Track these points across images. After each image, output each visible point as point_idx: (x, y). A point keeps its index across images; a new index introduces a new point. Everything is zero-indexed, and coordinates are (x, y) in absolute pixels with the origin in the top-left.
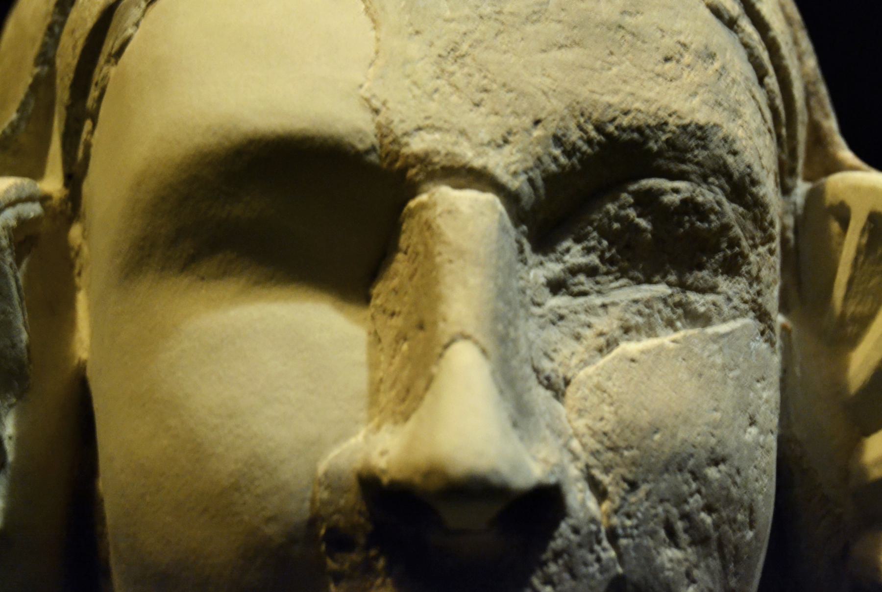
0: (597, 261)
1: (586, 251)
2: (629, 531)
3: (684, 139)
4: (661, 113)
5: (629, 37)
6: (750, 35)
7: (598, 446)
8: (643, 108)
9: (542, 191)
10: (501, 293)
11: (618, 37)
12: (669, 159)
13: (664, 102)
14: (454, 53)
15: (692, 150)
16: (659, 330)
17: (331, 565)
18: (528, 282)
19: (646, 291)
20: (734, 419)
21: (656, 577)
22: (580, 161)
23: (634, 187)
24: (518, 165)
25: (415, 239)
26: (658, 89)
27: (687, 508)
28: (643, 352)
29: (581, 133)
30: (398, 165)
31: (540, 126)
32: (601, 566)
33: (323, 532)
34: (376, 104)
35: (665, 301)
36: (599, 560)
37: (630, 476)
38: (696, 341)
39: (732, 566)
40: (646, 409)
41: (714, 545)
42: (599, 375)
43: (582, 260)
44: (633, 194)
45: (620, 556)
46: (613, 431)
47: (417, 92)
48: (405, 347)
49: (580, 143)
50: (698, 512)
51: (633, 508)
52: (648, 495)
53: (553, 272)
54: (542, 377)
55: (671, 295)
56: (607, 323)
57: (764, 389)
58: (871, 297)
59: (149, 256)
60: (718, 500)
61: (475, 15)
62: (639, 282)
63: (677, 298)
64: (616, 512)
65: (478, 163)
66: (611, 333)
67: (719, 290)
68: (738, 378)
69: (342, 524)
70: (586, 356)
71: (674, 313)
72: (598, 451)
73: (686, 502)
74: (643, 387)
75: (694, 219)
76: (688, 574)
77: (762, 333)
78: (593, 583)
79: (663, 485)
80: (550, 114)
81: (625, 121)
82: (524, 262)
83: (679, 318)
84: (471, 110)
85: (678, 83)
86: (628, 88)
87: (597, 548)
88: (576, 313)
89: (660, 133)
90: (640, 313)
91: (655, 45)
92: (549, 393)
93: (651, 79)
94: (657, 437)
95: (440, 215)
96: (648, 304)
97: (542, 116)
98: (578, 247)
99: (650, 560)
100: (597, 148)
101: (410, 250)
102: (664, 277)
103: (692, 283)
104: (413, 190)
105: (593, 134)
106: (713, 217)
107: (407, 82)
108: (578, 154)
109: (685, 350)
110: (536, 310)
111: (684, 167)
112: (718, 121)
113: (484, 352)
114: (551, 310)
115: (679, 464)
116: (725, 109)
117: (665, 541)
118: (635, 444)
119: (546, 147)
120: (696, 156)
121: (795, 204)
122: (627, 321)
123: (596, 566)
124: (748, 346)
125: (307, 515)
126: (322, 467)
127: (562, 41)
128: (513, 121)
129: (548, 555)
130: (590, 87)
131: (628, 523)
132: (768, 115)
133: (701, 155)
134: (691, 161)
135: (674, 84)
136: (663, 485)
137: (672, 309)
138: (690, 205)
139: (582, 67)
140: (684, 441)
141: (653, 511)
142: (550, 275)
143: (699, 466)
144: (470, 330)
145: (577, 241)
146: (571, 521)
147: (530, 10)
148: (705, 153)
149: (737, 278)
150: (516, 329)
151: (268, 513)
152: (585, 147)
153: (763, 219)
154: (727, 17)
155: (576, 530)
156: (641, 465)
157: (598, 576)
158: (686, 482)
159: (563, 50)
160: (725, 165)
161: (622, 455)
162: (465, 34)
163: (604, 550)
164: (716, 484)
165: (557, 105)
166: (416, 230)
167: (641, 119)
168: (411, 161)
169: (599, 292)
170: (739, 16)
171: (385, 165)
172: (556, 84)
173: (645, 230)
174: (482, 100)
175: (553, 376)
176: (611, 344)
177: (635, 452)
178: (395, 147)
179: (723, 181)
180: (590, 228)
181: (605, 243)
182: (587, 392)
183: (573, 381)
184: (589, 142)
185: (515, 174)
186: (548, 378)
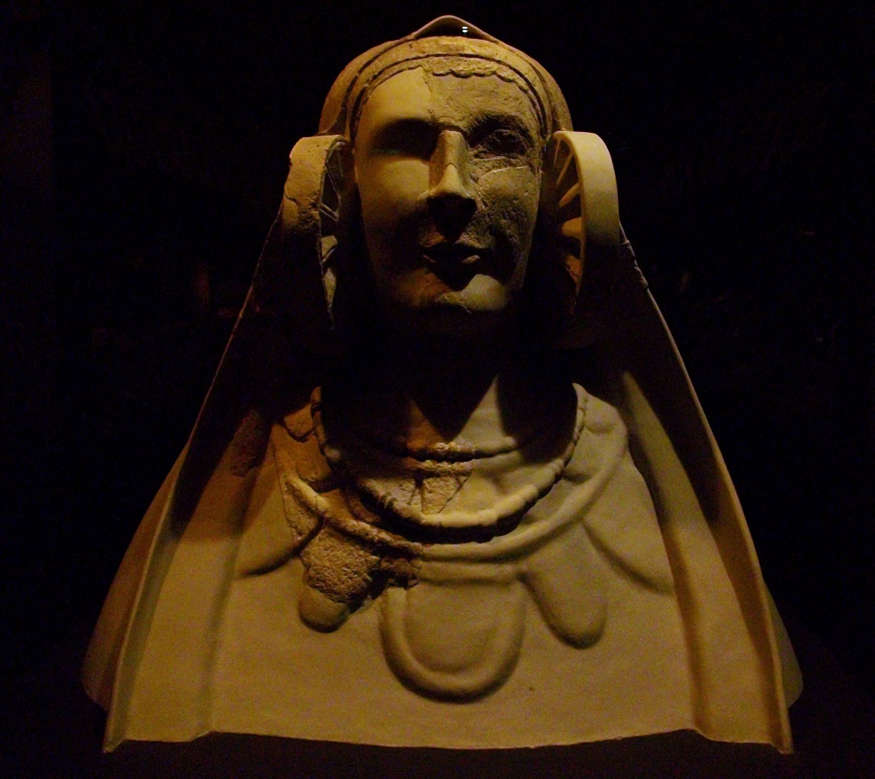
6: (531, 95)
9: (472, 132)
23: (496, 131)
34: (431, 111)
36: (485, 221)
43: (483, 150)
44: (496, 133)
52: (498, 206)
81: (493, 114)
82: (468, 149)
90: (497, 163)
96: (500, 160)
105: (485, 117)
109: (509, 172)
110: (471, 162)
126: (418, 199)
128: (465, 115)
131: (493, 212)
132: (536, 116)
133: (512, 123)
144: (452, 162)
152: (482, 121)
160: (520, 126)
176: (489, 170)
184: (484, 120)
186: (473, 178)
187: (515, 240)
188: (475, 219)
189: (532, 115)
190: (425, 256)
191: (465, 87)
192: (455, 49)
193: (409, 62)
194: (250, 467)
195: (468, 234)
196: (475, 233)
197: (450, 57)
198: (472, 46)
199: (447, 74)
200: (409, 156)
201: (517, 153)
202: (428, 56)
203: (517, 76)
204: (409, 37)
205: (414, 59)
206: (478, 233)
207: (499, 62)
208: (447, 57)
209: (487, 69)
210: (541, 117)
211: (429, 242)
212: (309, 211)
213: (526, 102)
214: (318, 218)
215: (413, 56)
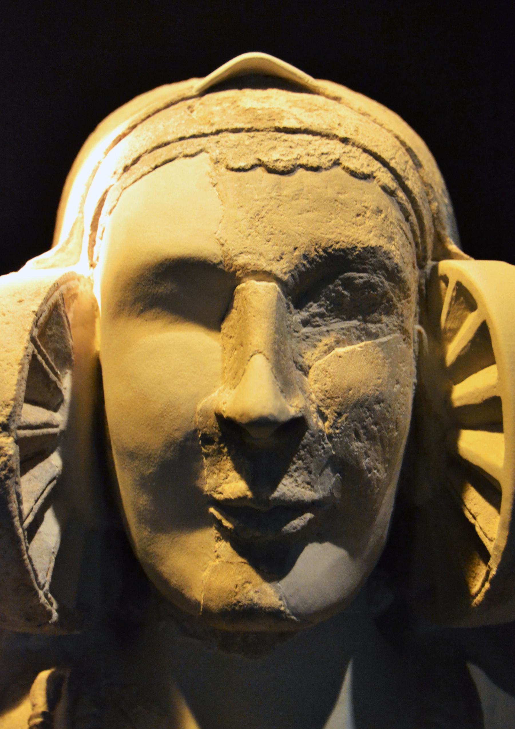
0: (324, 311)
1: (319, 306)
2: (337, 435)
3: (365, 253)
4: (354, 242)
5: (340, 205)
6: (401, 198)
7: (323, 397)
8: (345, 240)
9: (298, 280)
10: (277, 331)
11: (335, 205)
12: (358, 263)
13: (355, 237)
14: (258, 216)
15: (369, 259)
16: (354, 341)
17: (204, 450)
18: (292, 321)
19: (347, 324)
20: (388, 382)
21: (350, 455)
22: (316, 266)
23: (342, 276)
25: (240, 304)
26: (353, 230)
28: (345, 353)
29: (316, 253)
30: (232, 270)
31: (297, 250)
32: (325, 451)
33: (200, 436)
34: (222, 241)
35: (356, 328)
36: (323, 448)
37: (338, 410)
39: (387, 449)
43: (318, 310)
44: (341, 280)
47: (241, 236)
48: (236, 353)
49: (316, 257)
50: (370, 425)
52: (346, 418)
53: (304, 316)
54: (298, 365)
57: (404, 366)
58: (458, 320)
59: (123, 310)
61: (268, 197)
62: (344, 320)
63: (362, 327)
64: (331, 427)
65: (268, 269)
66: (330, 344)
67: (382, 322)
68: (390, 363)
69: (208, 433)
71: (361, 333)
72: (323, 399)
73: (364, 421)
74: (345, 369)
75: (370, 290)
76: (366, 453)
77: (404, 340)
78: (321, 458)
79: (354, 414)
80: (302, 245)
81: (337, 247)
82: (290, 313)
83: (363, 335)
84: (265, 244)
85: (363, 226)
86: (339, 231)
87: (322, 443)
88: (315, 335)
89: (353, 251)
90: (344, 334)
91: (352, 209)
92: (301, 373)
93: (349, 225)
94: (351, 392)
95: (250, 294)
96: (348, 329)
97: (298, 245)
98: (316, 305)
99: (347, 447)
100: (324, 260)
101: (238, 308)
104: (239, 281)
105: (322, 253)
106: (379, 289)
107: (237, 231)
108: (315, 263)
110: (296, 334)
111: (365, 267)
112: (381, 245)
113: (268, 359)
114: (303, 334)
116: (385, 238)
117: (354, 439)
118: (340, 396)
120: (370, 261)
121: (426, 273)
123: (322, 451)
124: (396, 347)
125: (193, 428)
126: (199, 407)
127: (309, 209)
128: (285, 249)
129: (300, 446)
130: (320, 231)
131: (337, 431)
132: (410, 235)
133: (373, 260)
135: (360, 227)
137: (360, 332)
139: (317, 221)
141: (349, 426)
142: (303, 318)
143: (371, 405)
144: (261, 349)
145: (315, 302)
146: (310, 432)
147: (294, 194)
148: (375, 260)
149: (391, 316)
150: (285, 345)
151: (176, 428)
152: (318, 259)
153: (404, 288)
154: (389, 190)
155: (313, 436)
157: (323, 455)
158: (365, 412)
159: (309, 213)
160: (385, 264)
161: (334, 401)
162: (263, 207)
163: (326, 444)
164: (378, 413)
166: (240, 300)
167: (344, 246)
168: (238, 268)
169: (326, 325)
170: (396, 189)
171: (226, 270)
172: (305, 230)
173: (347, 296)
174: (271, 239)
175: (303, 365)
176: (331, 349)
177: (340, 399)
178: (231, 262)
180: (321, 296)
181: (328, 302)
182: (319, 372)
186: (301, 366)
187: (378, 474)
188: (304, 447)
189: (404, 237)
190: (212, 510)
191: (284, 193)
192: (267, 117)
193: (185, 142)
195: (291, 476)
196: (305, 473)
197: (257, 133)
198: (295, 111)
199: (253, 167)
202: (218, 132)
203: (377, 165)
205: (194, 136)
206: (310, 472)
207: (345, 141)
208: (252, 134)
210: (418, 233)
211: (220, 489)
213: (395, 214)
214: (11, 452)
215: (193, 131)
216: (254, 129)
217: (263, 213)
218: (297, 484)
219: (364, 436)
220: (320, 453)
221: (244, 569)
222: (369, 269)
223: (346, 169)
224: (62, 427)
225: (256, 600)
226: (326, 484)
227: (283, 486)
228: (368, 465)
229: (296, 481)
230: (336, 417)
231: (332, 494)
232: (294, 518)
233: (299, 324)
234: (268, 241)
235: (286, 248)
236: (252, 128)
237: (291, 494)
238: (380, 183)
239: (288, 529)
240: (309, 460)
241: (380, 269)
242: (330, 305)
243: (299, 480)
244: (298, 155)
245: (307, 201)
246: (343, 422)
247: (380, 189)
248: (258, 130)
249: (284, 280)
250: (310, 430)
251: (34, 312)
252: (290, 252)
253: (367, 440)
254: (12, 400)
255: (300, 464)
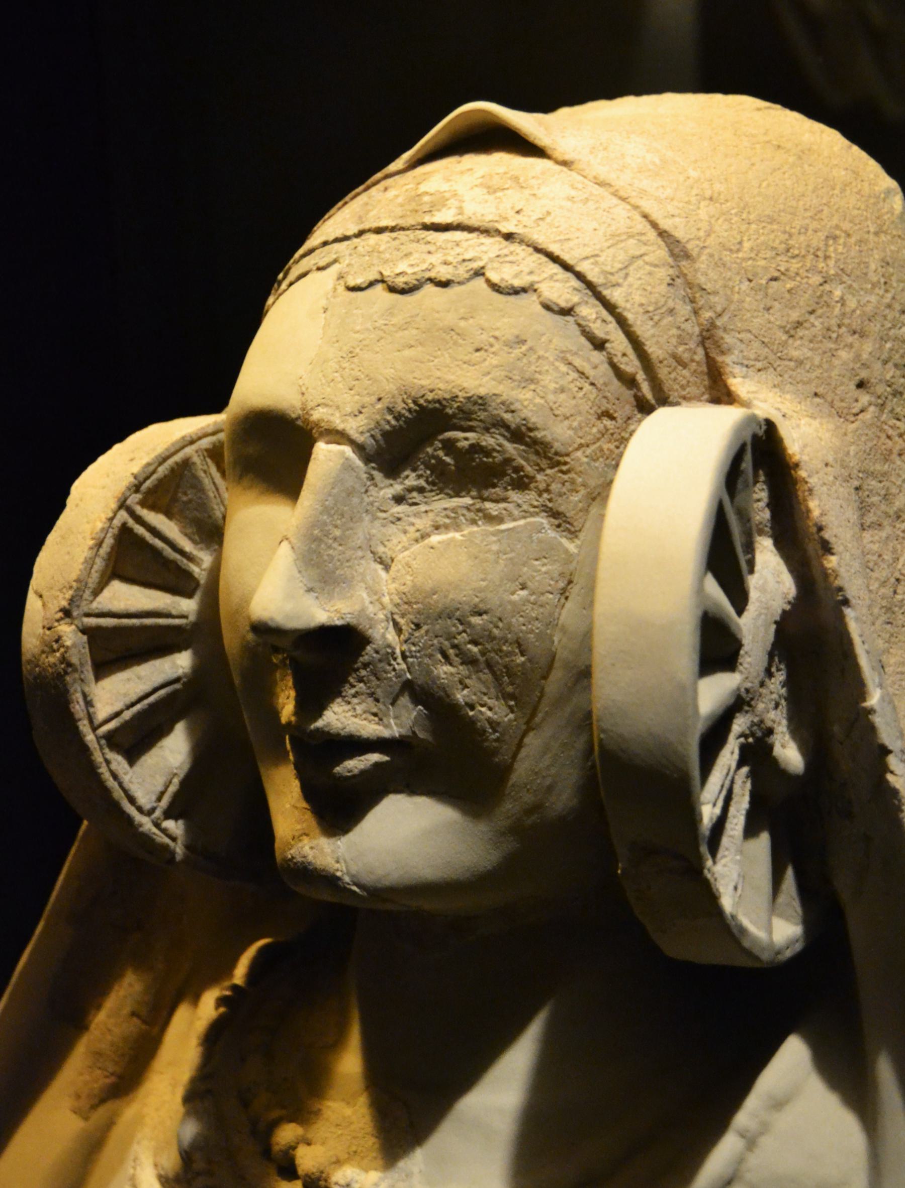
2: (414, 654)
3: (469, 406)
7: (399, 601)
9: (382, 442)
12: (460, 419)
13: (459, 382)
15: (476, 413)
18: (378, 497)
19: (454, 502)
22: (405, 422)
23: (441, 437)
24: (364, 427)
27: (456, 641)
28: (439, 543)
29: (404, 405)
30: (309, 427)
32: (396, 674)
36: (394, 670)
37: (415, 621)
38: (477, 535)
40: (431, 579)
41: (483, 666)
42: (409, 557)
43: (415, 483)
45: (409, 668)
46: (409, 592)
49: (404, 412)
50: (466, 645)
51: (417, 640)
52: (427, 632)
54: (376, 557)
55: (473, 504)
56: (423, 523)
60: (481, 638)
62: (451, 497)
63: (478, 506)
64: (406, 642)
65: (340, 427)
70: (406, 544)
71: (477, 516)
74: (433, 565)
75: (481, 456)
79: (438, 627)
81: (430, 396)
83: (480, 519)
87: (393, 662)
89: (453, 403)
90: (448, 517)
94: (435, 597)
96: (454, 510)
98: (414, 475)
100: (414, 414)
102: (468, 493)
103: (488, 497)
105: (412, 405)
109: (470, 540)
111: (471, 423)
114: (392, 515)
115: (448, 615)
117: (441, 662)
119: (384, 414)
120: (479, 416)
122: (437, 521)
123: (393, 673)
129: (359, 664)
131: (413, 648)
133: (482, 415)
134: (476, 420)
135: (473, 368)
136: (438, 627)
138: (478, 448)
140: (453, 600)
141: (430, 643)
145: (414, 470)
146: (374, 646)
148: (486, 414)
149: (527, 492)
152: (407, 414)
156: (423, 614)
157: (394, 679)
158: (454, 625)
160: (502, 420)
161: (412, 608)
165: (391, 387)
167: (440, 395)
169: (426, 503)
171: (305, 427)
173: (449, 464)
174: (354, 386)
175: (384, 556)
176: (424, 536)
177: (420, 606)
179: (503, 431)
181: (428, 472)
182: (400, 567)
183: (395, 560)
184: (410, 410)
185: (362, 433)
186: (380, 558)
188: (365, 666)
194: (103, 1101)
196: (370, 700)
199: (371, 284)
200: (279, 492)
201: (506, 489)
204: (393, 167)
206: (377, 700)
209: (466, 263)
212: (56, 624)
216: (398, 227)
217: (358, 350)
218: (354, 714)
219: (457, 659)
220: (389, 675)
221: (306, 817)
222: (479, 426)
223: (488, 281)
224: (192, 618)
225: (310, 858)
226: (404, 719)
227: (333, 714)
228: (467, 700)
229: (355, 709)
230: (412, 629)
231: (414, 733)
232: (351, 757)
233: (389, 501)
234: (351, 389)
235: (368, 399)
236: (397, 225)
237: (339, 725)
238: (541, 299)
239: (341, 772)
240: (373, 684)
241: (494, 425)
242: (431, 475)
243: (359, 709)
244: (431, 264)
245: (414, 332)
246: (422, 637)
247: (539, 307)
248: (403, 229)
249: (360, 442)
250: (374, 644)
251: (132, 474)
252: (372, 405)
253: (462, 664)
254: (74, 581)
255: (361, 688)
